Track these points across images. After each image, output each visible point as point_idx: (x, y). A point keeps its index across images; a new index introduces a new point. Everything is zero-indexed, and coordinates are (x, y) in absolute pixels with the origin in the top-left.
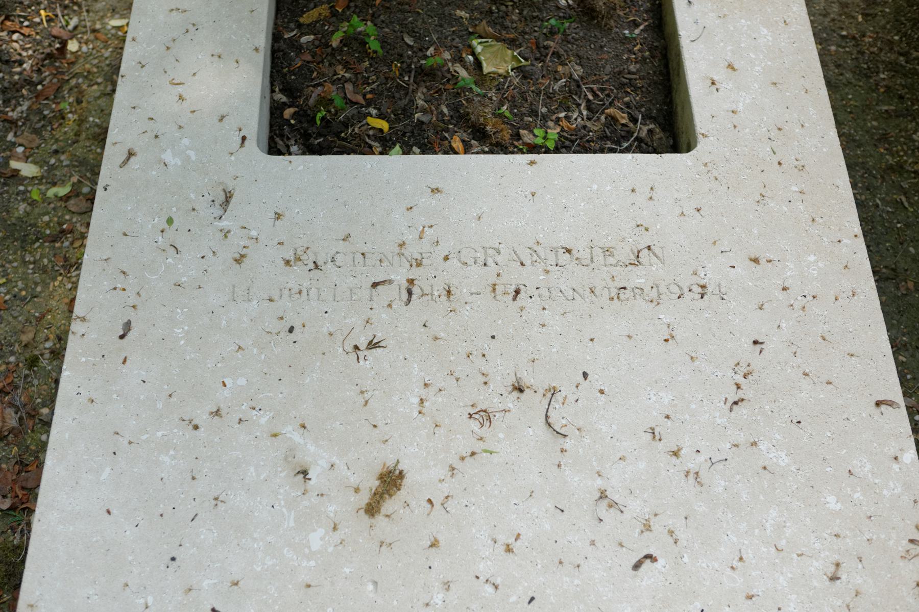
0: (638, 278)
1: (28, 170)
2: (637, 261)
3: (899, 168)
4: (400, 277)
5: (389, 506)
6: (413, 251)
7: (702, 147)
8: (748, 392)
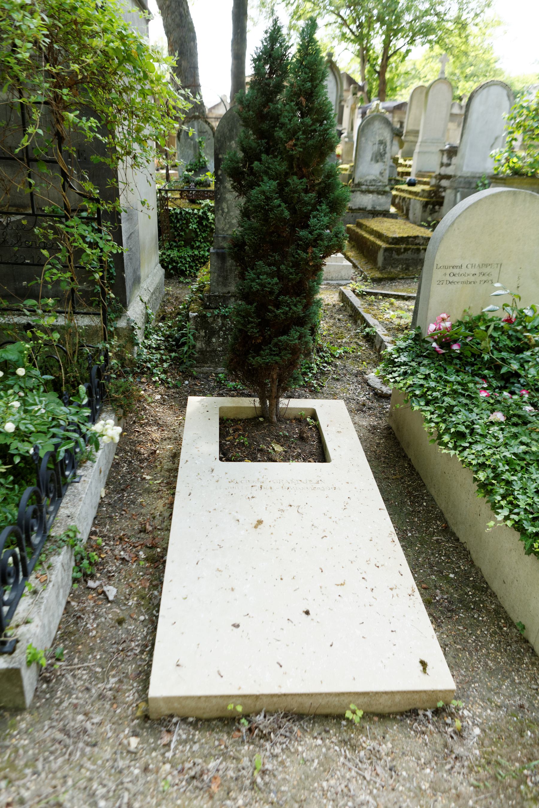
0: (317, 486)
1: (148, 477)
2: (318, 482)
3: (388, 478)
4: (259, 485)
5: (259, 527)
6: (261, 480)
7: (332, 462)
8: (347, 506)
